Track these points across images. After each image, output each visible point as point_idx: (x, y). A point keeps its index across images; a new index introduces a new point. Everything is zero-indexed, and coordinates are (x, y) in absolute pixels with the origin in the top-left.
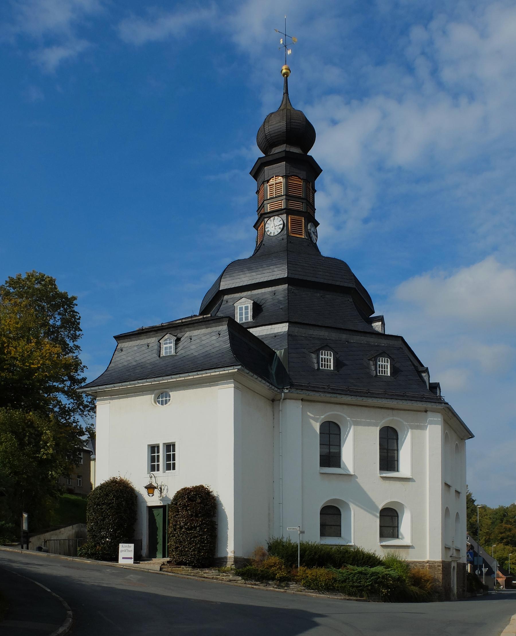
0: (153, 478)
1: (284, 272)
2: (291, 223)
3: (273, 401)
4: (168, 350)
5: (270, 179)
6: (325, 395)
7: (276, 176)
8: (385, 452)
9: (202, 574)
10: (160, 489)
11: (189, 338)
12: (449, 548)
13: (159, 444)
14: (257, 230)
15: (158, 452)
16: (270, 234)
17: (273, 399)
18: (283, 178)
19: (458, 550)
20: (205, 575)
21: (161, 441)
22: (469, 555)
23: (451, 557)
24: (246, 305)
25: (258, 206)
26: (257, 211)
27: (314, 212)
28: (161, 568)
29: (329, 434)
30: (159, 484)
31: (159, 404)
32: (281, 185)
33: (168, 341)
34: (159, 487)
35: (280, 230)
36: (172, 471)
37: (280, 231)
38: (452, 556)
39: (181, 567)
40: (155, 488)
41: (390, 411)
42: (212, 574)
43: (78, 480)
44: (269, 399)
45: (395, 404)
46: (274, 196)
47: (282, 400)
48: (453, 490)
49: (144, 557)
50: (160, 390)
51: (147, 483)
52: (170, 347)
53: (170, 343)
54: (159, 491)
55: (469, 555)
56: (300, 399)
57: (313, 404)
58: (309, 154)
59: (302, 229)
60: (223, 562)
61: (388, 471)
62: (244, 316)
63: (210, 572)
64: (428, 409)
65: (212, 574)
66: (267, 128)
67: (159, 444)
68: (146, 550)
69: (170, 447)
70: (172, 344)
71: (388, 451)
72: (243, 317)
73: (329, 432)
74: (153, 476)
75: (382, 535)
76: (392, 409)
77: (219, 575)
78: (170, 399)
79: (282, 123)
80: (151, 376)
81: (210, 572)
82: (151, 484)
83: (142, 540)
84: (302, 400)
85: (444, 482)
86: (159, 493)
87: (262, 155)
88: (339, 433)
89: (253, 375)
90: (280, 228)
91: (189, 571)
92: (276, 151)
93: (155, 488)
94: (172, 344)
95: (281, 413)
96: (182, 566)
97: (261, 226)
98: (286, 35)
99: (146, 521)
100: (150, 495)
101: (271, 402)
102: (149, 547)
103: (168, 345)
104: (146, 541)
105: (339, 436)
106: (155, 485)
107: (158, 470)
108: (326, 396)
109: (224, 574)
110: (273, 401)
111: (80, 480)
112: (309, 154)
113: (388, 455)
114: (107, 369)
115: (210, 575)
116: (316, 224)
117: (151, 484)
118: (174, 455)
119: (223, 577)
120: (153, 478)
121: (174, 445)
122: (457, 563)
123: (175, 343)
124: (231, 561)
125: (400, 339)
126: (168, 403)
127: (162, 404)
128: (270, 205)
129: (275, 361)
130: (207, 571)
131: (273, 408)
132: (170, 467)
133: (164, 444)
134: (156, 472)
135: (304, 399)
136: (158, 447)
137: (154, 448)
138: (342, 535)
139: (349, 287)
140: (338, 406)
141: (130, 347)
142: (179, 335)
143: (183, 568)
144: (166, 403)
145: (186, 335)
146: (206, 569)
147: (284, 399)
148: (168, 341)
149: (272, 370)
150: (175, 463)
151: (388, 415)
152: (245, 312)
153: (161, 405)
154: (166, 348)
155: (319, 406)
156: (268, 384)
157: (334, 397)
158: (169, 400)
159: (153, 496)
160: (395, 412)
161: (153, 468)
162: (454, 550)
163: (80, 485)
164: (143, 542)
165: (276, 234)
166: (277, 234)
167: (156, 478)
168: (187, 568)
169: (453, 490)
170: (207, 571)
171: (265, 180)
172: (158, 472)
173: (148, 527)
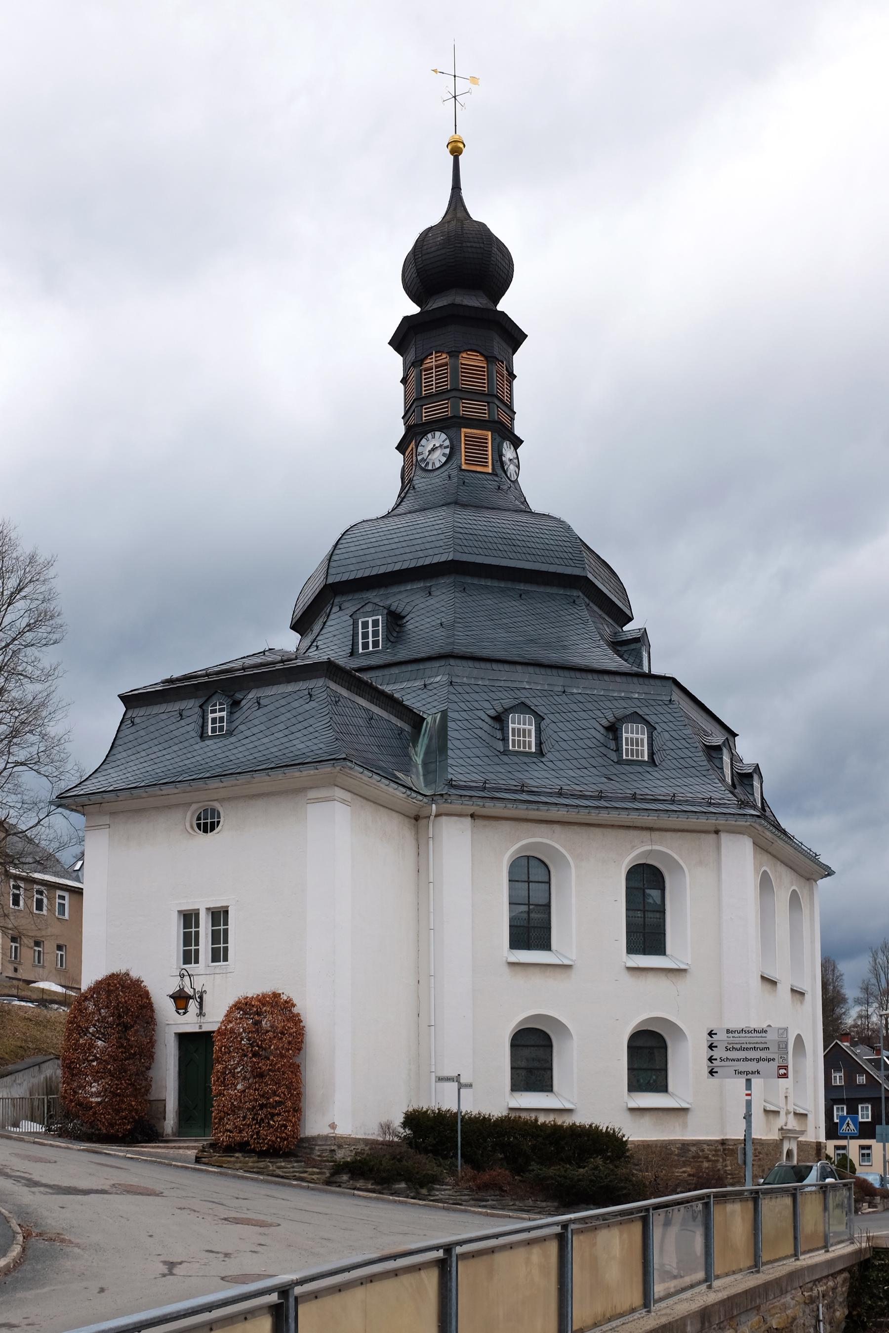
0: (187, 979)
1: (446, 551)
2: (466, 444)
3: (417, 818)
4: (218, 725)
5: (426, 358)
6: (515, 806)
7: (436, 353)
8: (639, 915)
9: (274, 1171)
10: (199, 1000)
11: (256, 701)
12: (777, 1113)
13: (199, 909)
14: (404, 454)
15: (197, 926)
16: (426, 466)
17: (417, 815)
18: (450, 356)
19: (802, 1116)
20: (279, 1172)
21: (202, 904)
22: (850, 1122)
23: (781, 1129)
24: (374, 618)
25: (405, 407)
26: (403, 418)
27: (512, 419)
28: (197, 1157)
29: (529, 882)
30: (198, 989)
31: (200, 830)
32: (447, 369)
33: (218, 707)
34: (197, 996)
35: (445, 459)
36: (222, 963)
37: (444, 459)
38: (784, 1127)
39: (233, 1156)
40: (191, 997)
41: (646, 834)
42: (291, 1170)
43: (57, 954)
44: (408, 816)
45: (655, 820)
46: (434, 390)
47: (432, 818)
48: (784, 990)
49: (168, 1135)
50: (199, 804)
51: (173, 988)
52: (221, 719)
53: (221, 710)
54: (197, 1004)
55: (850, 1122)
56: (467, 815)
57: (494, 823)
58: (500, 307)
59: (487, 455)
60: (313, 1145)
61: (645, 954)
62: (370, 640)
63: (289, 1166)
64: (720, 828)
65: (291, 1170)
66: (420, 259)
67: (199, 909)
68: (172, 1122)
69: (219, 916)
70: (225, 713)
71: (644, 915)
72: (368, 641)
73: (529, 878)
74: (186, 974)
75: (636, 1084)
76: (651, 829)
77: (306, 1172)
78: (219, 821)
79: (448, 250)
80: (185, 776)
81: (289, 1166)
82: (182, 990)
83: (165, 1100)
84: (472, 816)
85: (760, 973)
86: (199, 1007)
87: (413, 309)
88: (547, 880)
89: (371, 775)
90: (444, 455)
91: (250, 1164)
92: (435, 306)
93: (191, 997)
94: (225, 713)
95: (431, 842)
96: (237, 1155)
97: (410, 449)
98: (455, 76)
99: (174, 1063)
100: (180, 1011)
101: (413, 821)
102: (179, 1114)
103: (218, 715)
104: (172, 1103)
105: (548, 884)
106: (190, 992)
107: (197, 962)
108: (516, 808)
109: (315, 1170)
110: (417, 818)
111: (62, 955)
112: (500, 307)
113: (644, 922)
114: (105, 760)
115: (289, 1172)
116: (517, 442)
117: (182, 990)
118: (226, 931)
119: (313, 1177)
120: (187, 979)
121: (226, 912)
122: (798, 1141)
123: (229, 710)
124: (329, 1143)
125: (671, 681)
126: (217, 830)
127: (205, 831)
128: (425, 409)
129: (424, 735)
130: (283, 1164)
131: (417, 833)
132: (219, 955)
133: (208, 909)
134: (193, 965)
135: (476, 813)
136: (197, 914)
137: (189, 918)
138: (555, 1088)
139: (575, 576)
140: (544, 828)
141: (149, 717)
142: (239, 696)
143: (237, 1158)
144: (212, 829)
145: (250, 696)
146: (282, 1160)
147: (436, 816)
148: (218, 707)
149: (417, 755)
150: (227, 947)
151: (642, 842)
152: (368, 639)
153: (203, 832)
154: (214, 721)
155: (507, 826)
156: (404, 790)
157: (534, 809)
158: (218, 822)
159: (185, 1013)
160: (656, 835)
161: (190, 957)
162: (791, 1116)
163: (61, 965)
164: (167, 1105)
165: (437, 467)
166: (439, 465)
167: (192, 978)
168: (245, 1157)
169: (784, 990)
170: (283, 1164)
171: (418, 359)
172: (196, 965)
173: (177, 1075)
